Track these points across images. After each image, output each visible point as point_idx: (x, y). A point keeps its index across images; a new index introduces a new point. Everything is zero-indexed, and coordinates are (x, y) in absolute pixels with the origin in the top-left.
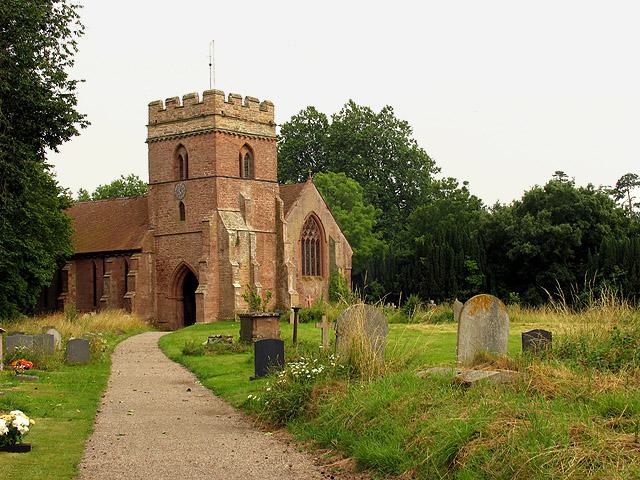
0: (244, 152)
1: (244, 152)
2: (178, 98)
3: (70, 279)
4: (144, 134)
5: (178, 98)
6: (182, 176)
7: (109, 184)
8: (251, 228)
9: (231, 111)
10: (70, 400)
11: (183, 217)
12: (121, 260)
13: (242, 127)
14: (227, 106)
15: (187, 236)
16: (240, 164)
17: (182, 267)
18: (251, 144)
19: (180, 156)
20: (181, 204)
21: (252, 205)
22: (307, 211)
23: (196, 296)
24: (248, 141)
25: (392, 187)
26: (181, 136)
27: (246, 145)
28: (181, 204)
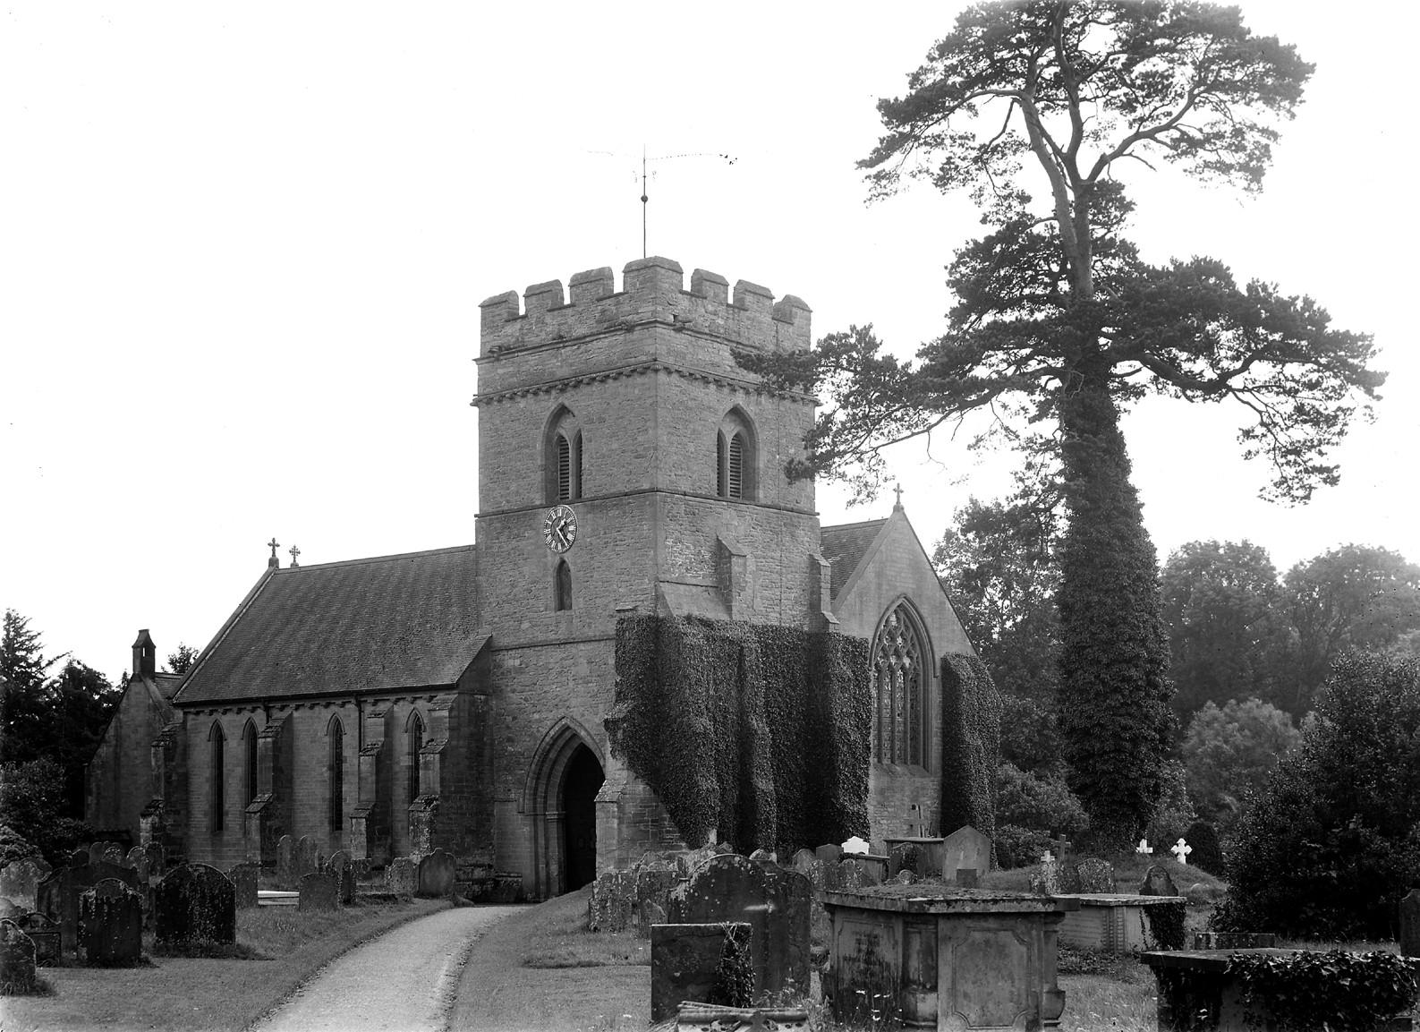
0: (730, 430)
1: (730, 430)
4: (468, 381)
5: (557, 283)
9: (702, 315)
26: (564, 385)
27: (736, 412)
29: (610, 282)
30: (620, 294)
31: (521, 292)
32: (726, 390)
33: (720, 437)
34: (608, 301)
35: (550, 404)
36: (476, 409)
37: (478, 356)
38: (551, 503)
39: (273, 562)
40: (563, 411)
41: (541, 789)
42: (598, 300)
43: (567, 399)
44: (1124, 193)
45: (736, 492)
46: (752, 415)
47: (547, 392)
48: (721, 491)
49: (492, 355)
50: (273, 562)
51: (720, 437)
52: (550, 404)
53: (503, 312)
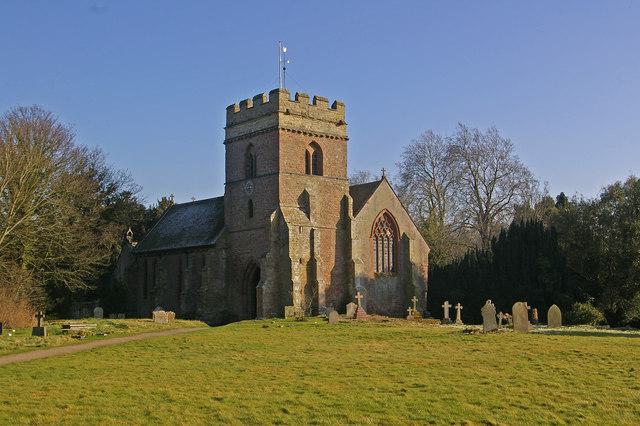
1: (311, 151)
13: (308, 125)
21: (316, 203)
27: (313, 144)
33: (307, 153)
35: (247, 142)
43: (253, 141)
48: (308, 172)
51: (307, 153)
52: (247, 142)
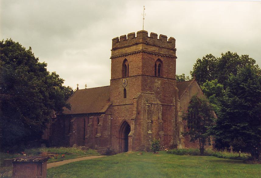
0: (158, 64)
2: (125, 35)
3: (74, 126)
4: (110, 54)
5: (125, 35)
6: (126, 75)
7: (16, 42)
8: (159, 103)
9: (151, 42)
10: (26, 111)
11: (125, 97)
12: (96, 118)
14: (149, 39)
15: (126, 106)
16: (156, 69)
17: (123, 123)
18: (162, 59)
19: (126, 65)
20: (125, 90)
22: (192, 95)
23: (129, 138)
24: (160, 57)
25: (170, 67)
26: (126, 55)
27: (159, 60)
28: (125, 90)
29: (113, 43)
30: (136, 38)
31: (119, 37)
32: (157, 56)
33: (156, 65)
34: (134, 39)
35: (123, 58)
36: (111, 59)
37: (111, 49)
38: (123, 78)
39: (78, 88)
40: (126, 60)
41: (123, 126)
42: (132, 39)
43: (127, 58)
44: (38, 61)
45: (159, 75)
46: (162, 60)
47: (123, 56)
49: (114, 49)
50: (78, 88)
53: (116, 41)
